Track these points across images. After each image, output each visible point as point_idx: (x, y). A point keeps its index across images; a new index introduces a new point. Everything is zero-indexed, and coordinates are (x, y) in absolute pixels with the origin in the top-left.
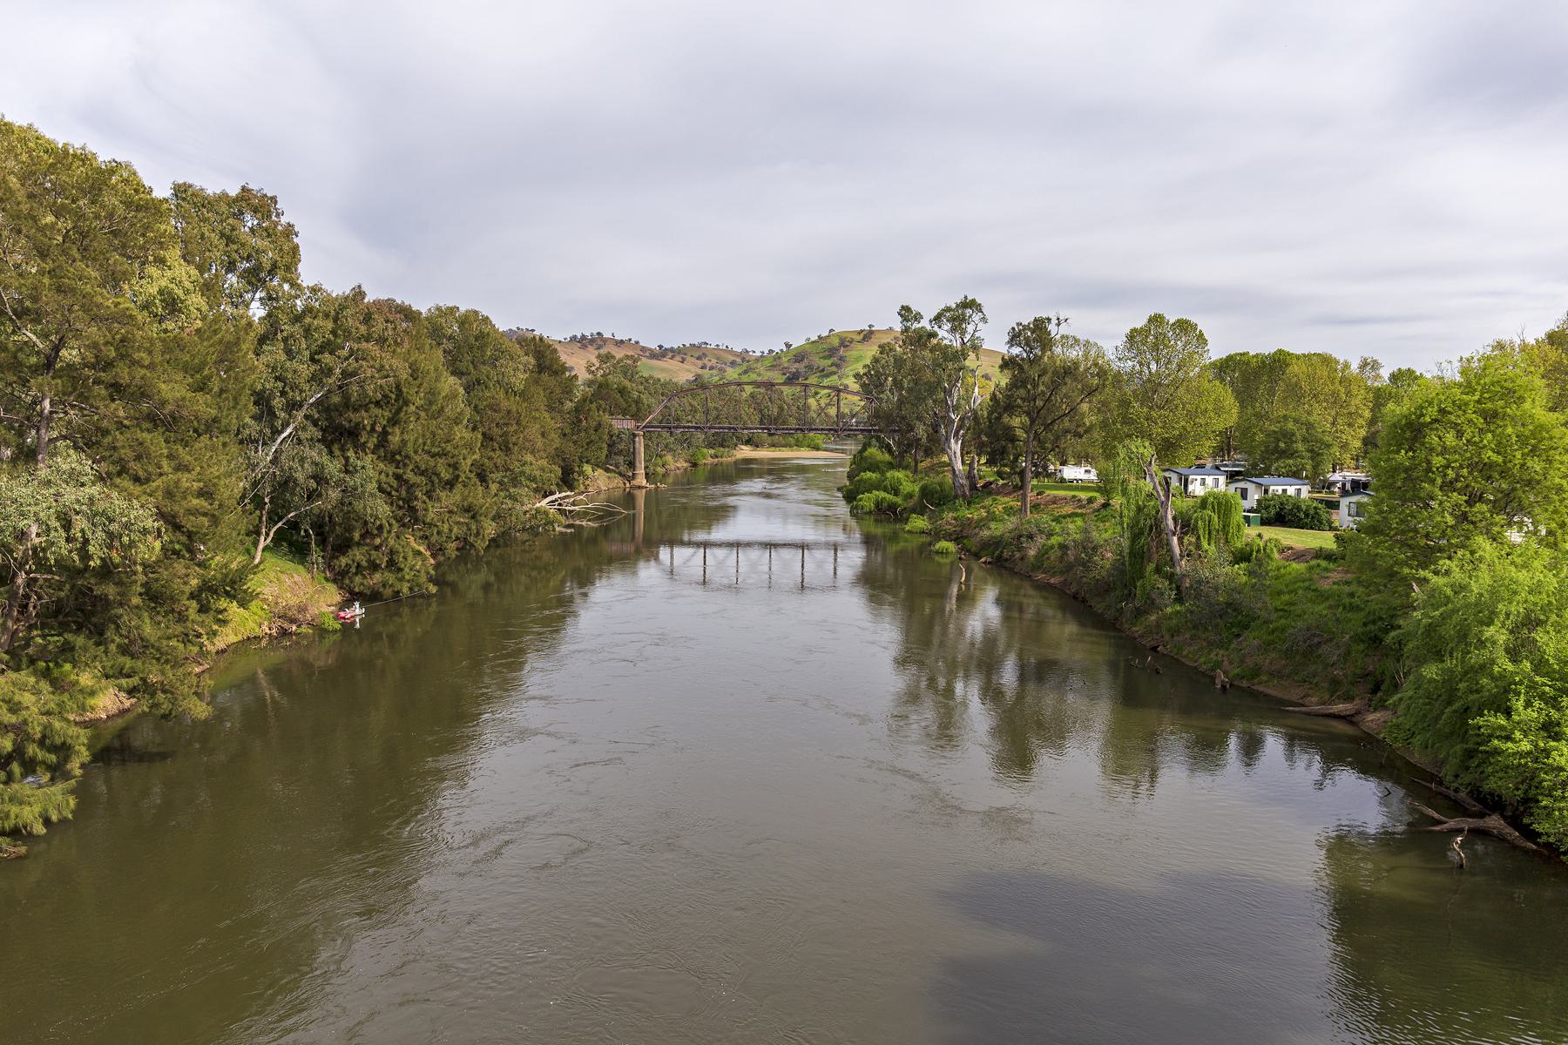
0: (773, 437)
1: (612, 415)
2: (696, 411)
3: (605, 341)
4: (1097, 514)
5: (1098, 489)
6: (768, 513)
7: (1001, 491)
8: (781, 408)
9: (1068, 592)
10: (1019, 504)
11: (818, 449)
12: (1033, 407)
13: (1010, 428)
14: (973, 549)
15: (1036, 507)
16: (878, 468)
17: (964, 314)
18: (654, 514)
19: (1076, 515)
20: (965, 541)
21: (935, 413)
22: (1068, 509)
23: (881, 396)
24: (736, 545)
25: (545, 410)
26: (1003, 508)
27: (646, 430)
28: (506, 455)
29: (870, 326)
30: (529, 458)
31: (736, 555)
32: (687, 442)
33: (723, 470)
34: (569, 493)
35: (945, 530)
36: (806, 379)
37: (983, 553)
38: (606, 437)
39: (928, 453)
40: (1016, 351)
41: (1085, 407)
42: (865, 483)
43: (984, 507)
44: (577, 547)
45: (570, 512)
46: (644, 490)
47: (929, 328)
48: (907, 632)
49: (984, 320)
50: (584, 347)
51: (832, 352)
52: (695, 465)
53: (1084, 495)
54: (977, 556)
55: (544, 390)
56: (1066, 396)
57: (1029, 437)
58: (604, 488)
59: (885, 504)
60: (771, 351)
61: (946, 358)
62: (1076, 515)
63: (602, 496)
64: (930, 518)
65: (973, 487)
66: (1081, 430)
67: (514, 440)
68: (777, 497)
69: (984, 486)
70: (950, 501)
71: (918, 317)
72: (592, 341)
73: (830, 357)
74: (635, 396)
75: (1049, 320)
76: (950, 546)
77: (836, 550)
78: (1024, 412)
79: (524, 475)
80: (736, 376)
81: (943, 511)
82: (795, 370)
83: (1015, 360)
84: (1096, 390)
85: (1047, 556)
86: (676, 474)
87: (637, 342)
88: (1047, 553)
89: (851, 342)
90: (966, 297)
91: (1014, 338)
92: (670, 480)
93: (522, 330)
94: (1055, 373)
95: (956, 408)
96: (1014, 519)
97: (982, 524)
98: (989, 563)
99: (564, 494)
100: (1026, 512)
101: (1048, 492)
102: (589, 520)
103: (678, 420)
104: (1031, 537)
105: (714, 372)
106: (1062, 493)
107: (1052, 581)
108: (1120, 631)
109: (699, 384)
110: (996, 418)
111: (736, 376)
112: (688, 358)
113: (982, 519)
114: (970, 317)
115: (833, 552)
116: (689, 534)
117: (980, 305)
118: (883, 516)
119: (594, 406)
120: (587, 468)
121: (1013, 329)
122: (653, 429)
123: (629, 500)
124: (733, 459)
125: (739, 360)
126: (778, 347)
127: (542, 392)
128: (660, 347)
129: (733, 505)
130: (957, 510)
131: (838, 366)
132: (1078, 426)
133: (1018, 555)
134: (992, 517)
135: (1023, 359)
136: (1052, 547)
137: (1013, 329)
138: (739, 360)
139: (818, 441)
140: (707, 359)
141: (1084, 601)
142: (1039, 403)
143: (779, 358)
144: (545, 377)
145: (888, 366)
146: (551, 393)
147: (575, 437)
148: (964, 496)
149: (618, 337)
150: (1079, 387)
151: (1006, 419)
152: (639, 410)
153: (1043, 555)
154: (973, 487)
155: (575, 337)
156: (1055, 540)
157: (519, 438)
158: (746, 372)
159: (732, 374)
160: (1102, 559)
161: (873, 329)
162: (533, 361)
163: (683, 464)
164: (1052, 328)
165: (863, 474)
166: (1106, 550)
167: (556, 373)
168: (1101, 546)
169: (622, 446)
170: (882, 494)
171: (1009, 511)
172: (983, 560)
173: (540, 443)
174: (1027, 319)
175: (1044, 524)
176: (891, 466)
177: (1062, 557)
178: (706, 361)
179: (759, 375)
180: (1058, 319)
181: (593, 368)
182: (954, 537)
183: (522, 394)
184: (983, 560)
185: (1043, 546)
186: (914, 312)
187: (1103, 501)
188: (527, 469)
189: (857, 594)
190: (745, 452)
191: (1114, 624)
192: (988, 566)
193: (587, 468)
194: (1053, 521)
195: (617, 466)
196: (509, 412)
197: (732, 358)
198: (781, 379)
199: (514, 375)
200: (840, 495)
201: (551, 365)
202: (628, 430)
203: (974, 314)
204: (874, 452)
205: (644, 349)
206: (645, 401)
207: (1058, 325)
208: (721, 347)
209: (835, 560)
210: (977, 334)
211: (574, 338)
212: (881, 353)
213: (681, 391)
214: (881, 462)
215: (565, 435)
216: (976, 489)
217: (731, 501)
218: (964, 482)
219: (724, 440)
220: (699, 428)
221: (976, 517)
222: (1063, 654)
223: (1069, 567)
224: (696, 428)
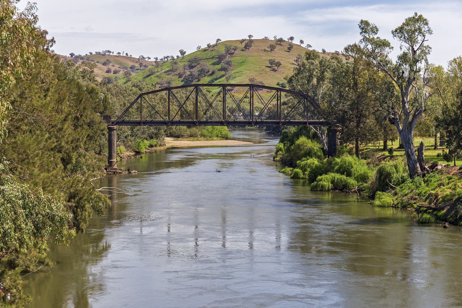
29: (250, 36)
49: (430, 31)
51: (220, 58)
52: (138, 153)
73: (218, 63)
89: (235, 50)
117: (425, 20)
125: (137, 65)
126: (176, 54)
128: (72, 55)
138: (137, 65)
140: (110, 64)
143: (176, 63)
161: (252, 38)
178: (110, 66)
189: (327, 271)
197: (131, 64)
208: (121, 55)
210: (425, 44)
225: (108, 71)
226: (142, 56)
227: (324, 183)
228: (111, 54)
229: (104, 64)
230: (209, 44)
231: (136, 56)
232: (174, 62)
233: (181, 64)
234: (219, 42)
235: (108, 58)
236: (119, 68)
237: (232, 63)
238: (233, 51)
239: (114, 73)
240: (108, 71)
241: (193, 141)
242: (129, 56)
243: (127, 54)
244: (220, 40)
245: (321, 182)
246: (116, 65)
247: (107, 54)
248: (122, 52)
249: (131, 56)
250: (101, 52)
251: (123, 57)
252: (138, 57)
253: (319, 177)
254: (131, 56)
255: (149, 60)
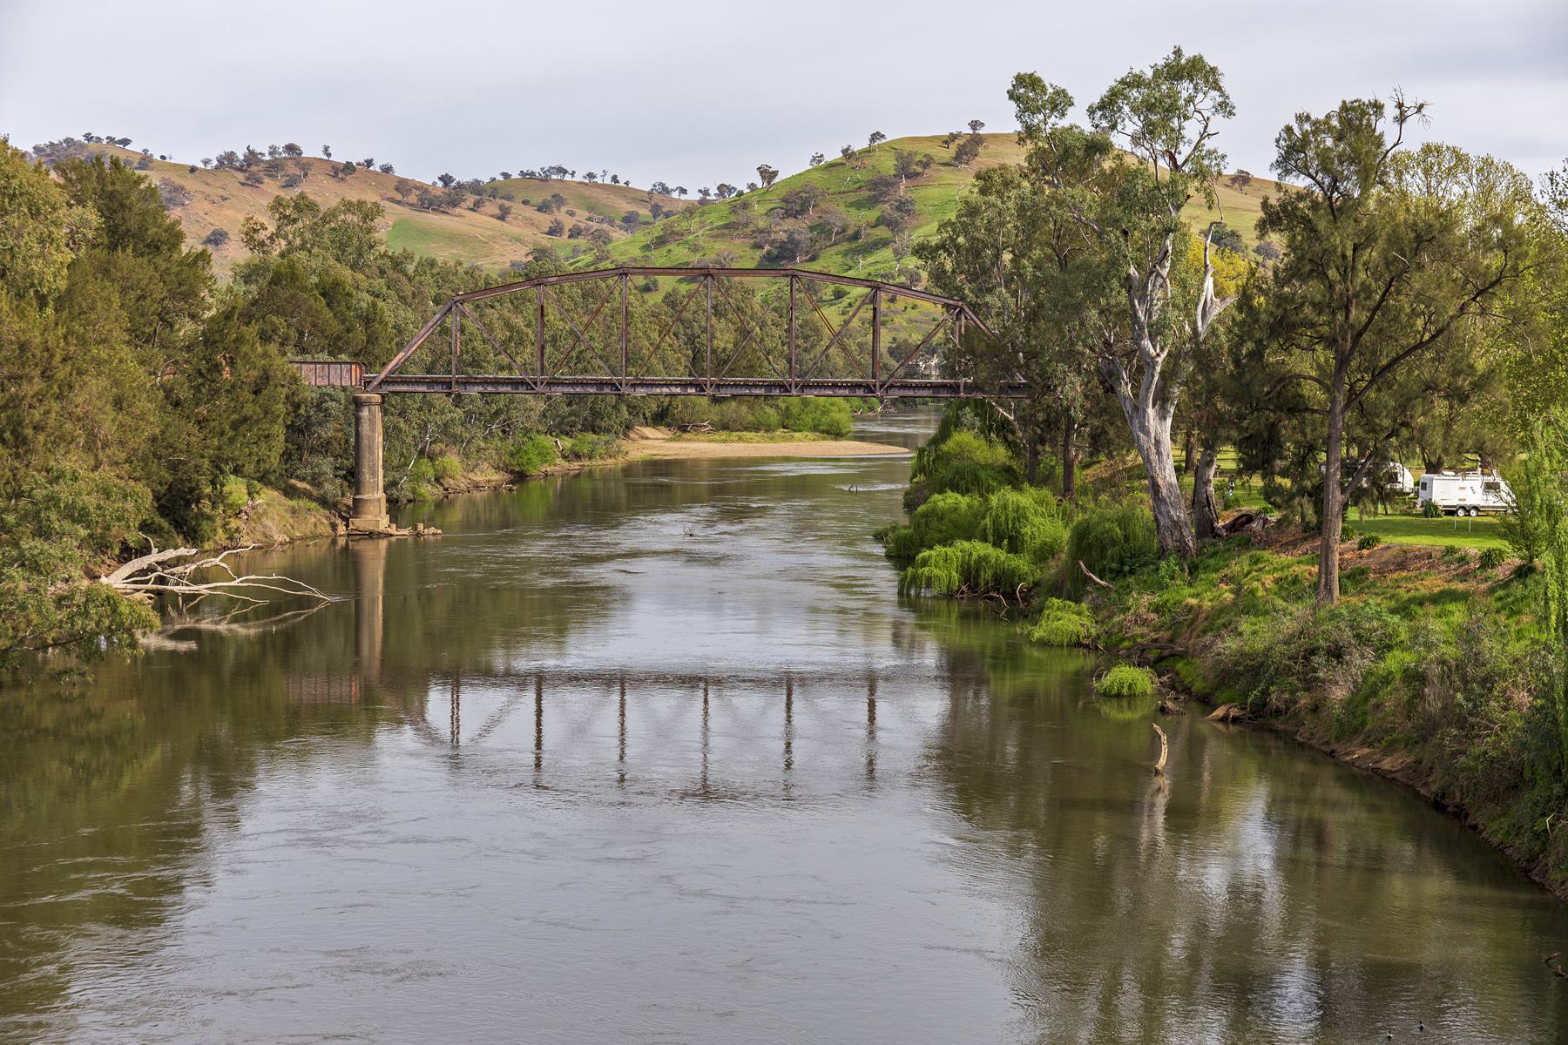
0: (725, 407)
1: (304, 351)
2: (521, 342)
3: (306, 166)
4: (1501, 593)
5: (1507, 532)
6: (716, 600)
7: (1275, 539)
8: (745, 333)
9: (1423, 791)
10: (1315, 569)
11: (836, 433)
12: (1341, 326)
13: (1286, 381)
14: (1198, 686)
15: (1355, 578)
16: (977, 480)
17: (1174, 96)
18: (414, 603)
19: (1453, 596)
20: (1179, 665)
21: (1107, 343)
22: (1434, 583)
23: (988, 298)
24: (618, 680)
25: (128, 343)
26: (1277, 581)
27: (386, 389)
28: (17, 456)
30: (72, 461)
31: (702, 705)
32: (501, 422)
33: (594, 492)
34: (182, 551)
35: (1133, 637)
36: (813, 259)
37: (1222, 695)
38: (281, 408)
39: (1099, 442)
40: (1299, 182)
41: (1472, 325)
42: (941, 519)
43: (1227, 579)
44: (206, 684)
45: (188, 598)
46: (383, 544)
47: (1087, 127)
48: (1046, 890)
49: (1225, 108)
50: (253, 182)
51: (878, 189)
52: (520, 477)
53: (1473, 547)
54: (1206, 702)
55: (124, 291)
56: (1419, 297)
57: (1333, 401)
58: (279, 538)
59: (986, 575)
60: (723, 189)
61: (1126, 198)
62: (1453, 596)
63: (276, 559)
64: (1095, 609)
65: (1206, 529)
66: (1464, 383)
67: (37, 417)
68: (716, 561)
69: (1234, 527)
70: (1145, 565)
71: (1060, 102)
72: (274, 167)
73: (872, 202)
74: (364, 305)
75: (1378, 107)
76: (1139, 678)
77: (872, 690)
78: (1321, 338)
79: (56, 505)
80: (636, 252)
81: (1127, 589)
82: (783, 236)
83: (1296, 208)
84: (1498, 281)
85: (1373, 701)
86: (471, 502)
87: (387, 169)
88: (1374, 693)
89: (926, 165)
90: (1178, 52)
91: (1293, 151)
92: (456, 515)
93: (99, 139)
94: (1394, 240)
95: (1157, 331)
96: (1299, 609)
97: (1220, 621)
98: (1235, 720)
99: (170, 554)
100: (1330, 591)
101: (1387, 539)
102: (235, 620)
103: (475, 363)
104: (1337, 653)
105: (582, 242)
106: (1422, 542)
107: (1386, 764)
108: (1542, 888)
109: (535, 275)
110: (1251, 354)
111: (636, 252)
112: (517, 208)
113: (1222, 610)
114: (1190, 100)
115: (866, 691)
116: (508, 655)
117: (1213, 70)
118: (981, 604)
119: (251, 331)
120: (236, 488)
121: (1289, 130)
122: (405, 388)
123: (347, 566)
124: (620, 461)
125: (645, 213)
126: (744, 179)
127: (116, 299)
128: (446, 180)
129: (603, 583)
130: (1162, 587)
131: (892, 224)
132: (1456, 373)
133: (1304, 699)
134: (1248, 605)
135: (1315, 206)
136: (1387, 679)
137: (1289, 130)
138: (645, 213)
139: (837, 416)
140: (564, 209)
141: (1460, 814)
142: (1358, 315)
143: (745, 206)
144: (126, 258)
145: (1002, 224)
146: (143, 297)
147: (203, 410)
148: (1182, 551)
149: (339, 157)
150: (1456, 274)
151: (1272, 358)
152: (372, 339)
153: (1366, 700)
154: (1206, 529)
155: (230, 156)
156: (1394, 661)
157: (47, 412)
158: (661, 242)
159: (625, 246)
160: (1506, 709)
161: (981, 131)
162: (94, 218)
163: (488, 475)
164: (1385, 126)
165: (936, 497)
166: (1515, 684)
167: (154, 247)
168: (1503, 675)
169: (328, 432)
170: (980, 549)
171: (1290, 587)
172: (1220, 712)
173: (108, 424)
174: (1323, 106)
175: (1370, 619)
176: (1011, 478)
177: (1410, 703)
178: (561, 215)
179: (695, 249)
180: (1400, 106)
181: (262, 235)
182: (1152, 655)
183: (64, 301)
184: (1220, 712)
185: (1365, 678)
186: (1050, 90)
187: (1518, 562)
188: (64, 492)
190: (653, 444)
191: (1527, 871)
192: (1233, 729)
193: (236, 488)
194: (1393, 611)
195: (316, 481)
196: (23, 347)
197: (626, 207)
198: (750, 259)
199: (42, 255)
200: (879, 550)
201: (143, 229)
202: (344, 389)
203: (1201, 96)
204: (968, 441)
205: (403, 186)
206: (389, 317)
207: (1401, 119)
208: (599, 180)
209: (872, 719)
210: (1209, 144)
211: (227, 160)
212: (983, 192)
213: (483, 290)
214: (983, 467)
215: (177, 404)
216: (1214, 533)
217: (605, 573)
218: (1181, 514)
219: (596, 414)
220: (522, 383)
221: (1207, 604)
222: (1430, 952)
223: (1429, 729)
224: (516, 384)
225: (554, 231)
226: (662, 185)
227: (936, 571)
228: (568, 177)
229: (543, 208)
230: (847, 150)
231: (643, 183)
232: (742, 204)
233: (759, 209)
234: (878, 142)
235: (556, 191)
236: (589, 219)
237: (917, 207)
238: (919, 169)
239: (570, 237)
240: (554, 231)
241: (725, 441)
242: (622, 184)
243: (615, 178)
244: (883, 136)
245: (926, 569)
246: (578, 212)
247: (553, 177)
248: (599, 173)
249: (627, 183)
250: (537, 170)
251: (603, 186)
252: (648, 188)
253: (925, 553)
254: (627, 183)
255: (683, 197)
